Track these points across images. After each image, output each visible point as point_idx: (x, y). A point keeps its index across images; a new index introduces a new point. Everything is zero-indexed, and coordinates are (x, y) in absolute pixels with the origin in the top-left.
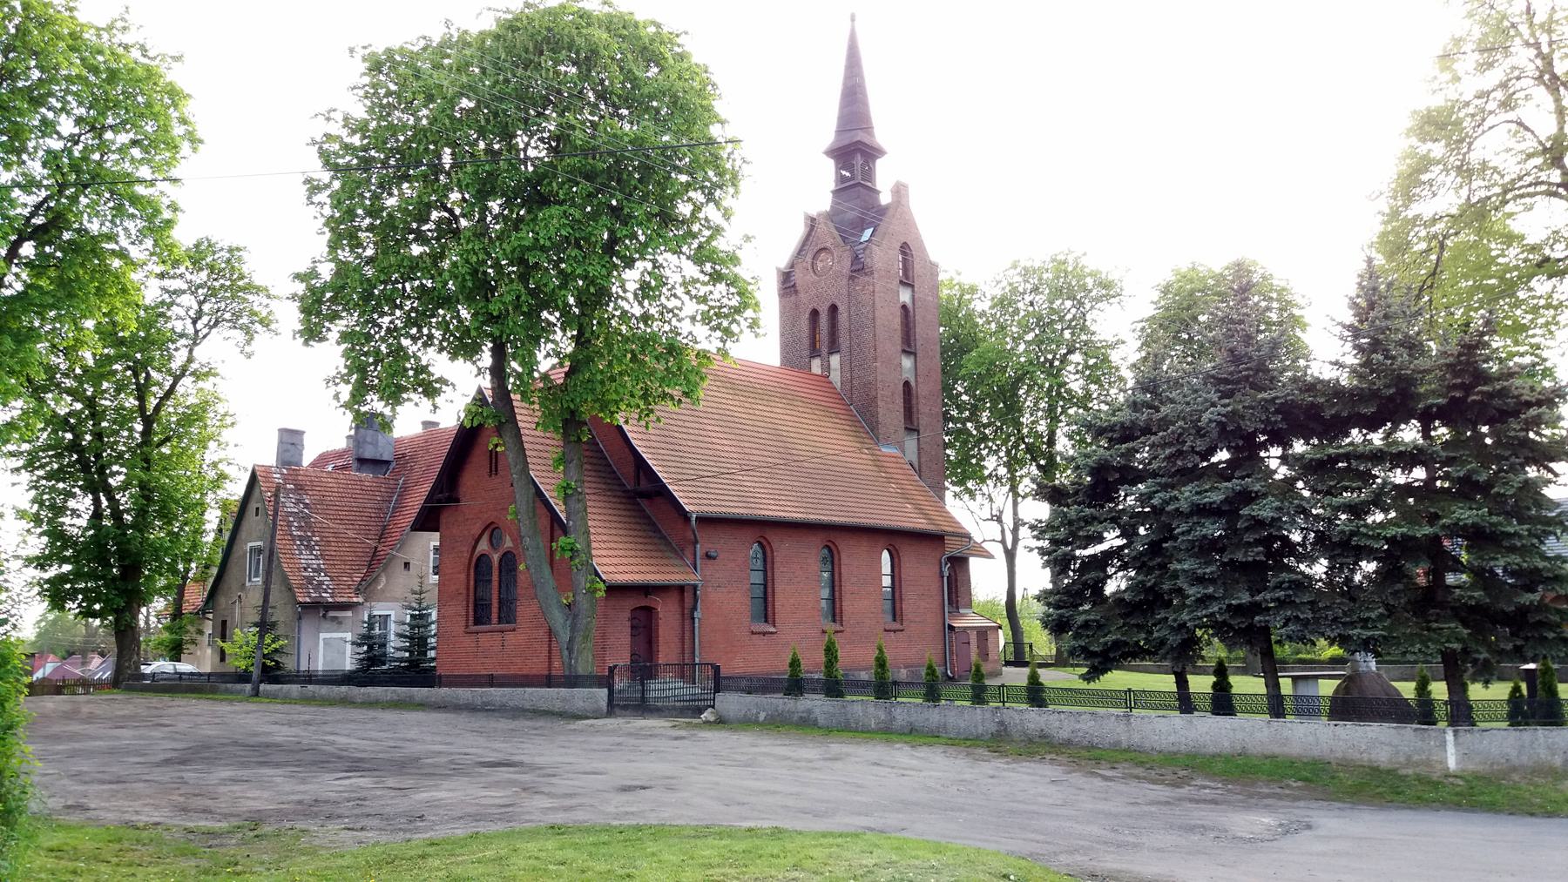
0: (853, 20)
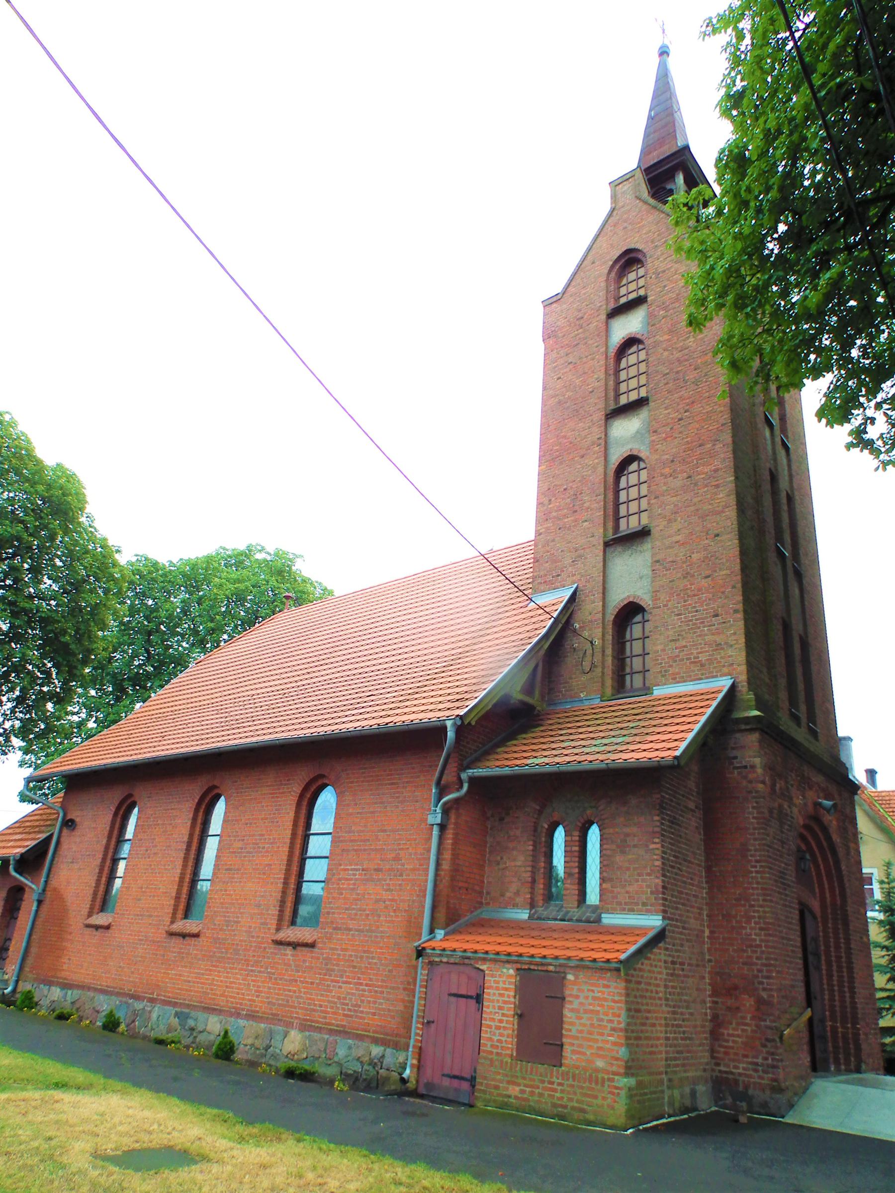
0: (664, 52)
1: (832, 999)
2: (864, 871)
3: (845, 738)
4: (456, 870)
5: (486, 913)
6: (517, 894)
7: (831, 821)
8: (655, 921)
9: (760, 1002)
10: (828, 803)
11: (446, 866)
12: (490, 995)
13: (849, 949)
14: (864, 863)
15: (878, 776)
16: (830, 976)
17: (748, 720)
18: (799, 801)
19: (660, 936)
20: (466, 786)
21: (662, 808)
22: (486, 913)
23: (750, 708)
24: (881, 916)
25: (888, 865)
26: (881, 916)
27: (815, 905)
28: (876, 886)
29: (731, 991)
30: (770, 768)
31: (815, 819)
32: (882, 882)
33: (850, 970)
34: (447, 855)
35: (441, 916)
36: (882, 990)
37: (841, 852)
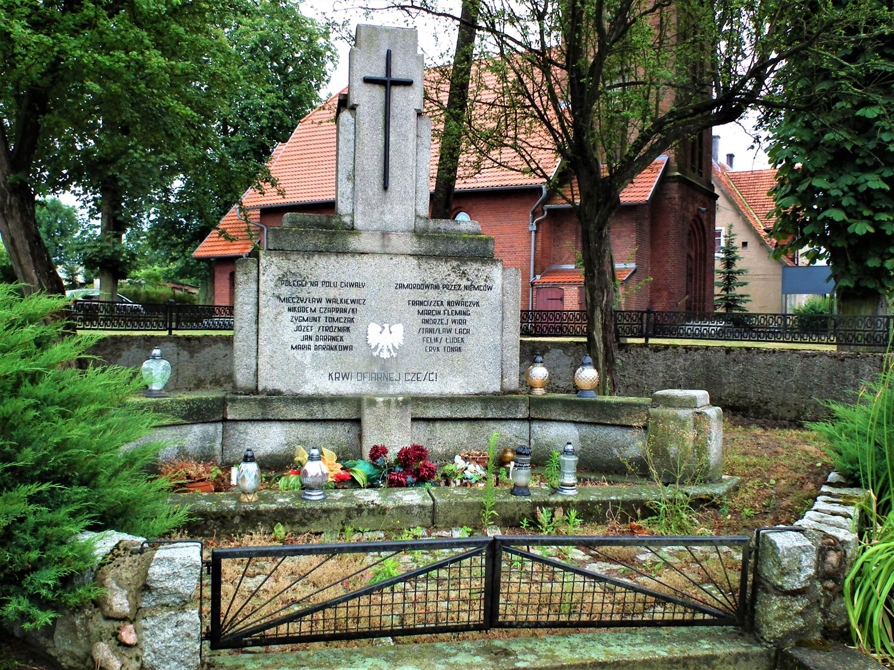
1: (695, 294)
2: (717, 228)
3: (715, 137)
4: (543, 250)
5: (554, 267)
6: (569, 258)
7: (704, 217)
8: (633, 266)
9: (670, 293)
10: (704, 209)
11: (539, 249)
12: (566, 298)
13: (705, 272)
14: (717, 223)
15: (735, 159)
16: (696, 284)
17: (674, 177)
18: (691, 210)
19: (635, 271)
20: (546, 213)
21: (637, 219)
22: (554, 267)
23: (675, 171)
24: (723, 256)
25: (731, 226)
26: (723, 256)
27: (693, 254)
28: (722, 239)
29: (658, 290)
30: (682, 198)
31: (698, 217)
32: (726, 236)
33: (705, 281)
34: (539, 244)
35: (538, 270)
36: (718, 295)
37: (706, 229)
